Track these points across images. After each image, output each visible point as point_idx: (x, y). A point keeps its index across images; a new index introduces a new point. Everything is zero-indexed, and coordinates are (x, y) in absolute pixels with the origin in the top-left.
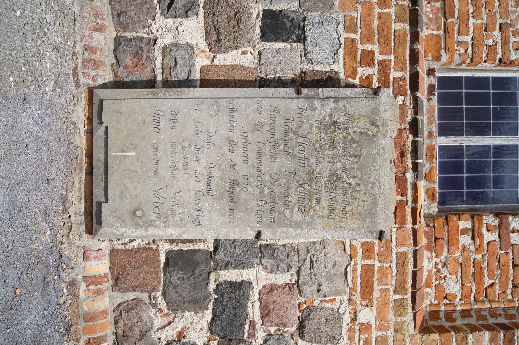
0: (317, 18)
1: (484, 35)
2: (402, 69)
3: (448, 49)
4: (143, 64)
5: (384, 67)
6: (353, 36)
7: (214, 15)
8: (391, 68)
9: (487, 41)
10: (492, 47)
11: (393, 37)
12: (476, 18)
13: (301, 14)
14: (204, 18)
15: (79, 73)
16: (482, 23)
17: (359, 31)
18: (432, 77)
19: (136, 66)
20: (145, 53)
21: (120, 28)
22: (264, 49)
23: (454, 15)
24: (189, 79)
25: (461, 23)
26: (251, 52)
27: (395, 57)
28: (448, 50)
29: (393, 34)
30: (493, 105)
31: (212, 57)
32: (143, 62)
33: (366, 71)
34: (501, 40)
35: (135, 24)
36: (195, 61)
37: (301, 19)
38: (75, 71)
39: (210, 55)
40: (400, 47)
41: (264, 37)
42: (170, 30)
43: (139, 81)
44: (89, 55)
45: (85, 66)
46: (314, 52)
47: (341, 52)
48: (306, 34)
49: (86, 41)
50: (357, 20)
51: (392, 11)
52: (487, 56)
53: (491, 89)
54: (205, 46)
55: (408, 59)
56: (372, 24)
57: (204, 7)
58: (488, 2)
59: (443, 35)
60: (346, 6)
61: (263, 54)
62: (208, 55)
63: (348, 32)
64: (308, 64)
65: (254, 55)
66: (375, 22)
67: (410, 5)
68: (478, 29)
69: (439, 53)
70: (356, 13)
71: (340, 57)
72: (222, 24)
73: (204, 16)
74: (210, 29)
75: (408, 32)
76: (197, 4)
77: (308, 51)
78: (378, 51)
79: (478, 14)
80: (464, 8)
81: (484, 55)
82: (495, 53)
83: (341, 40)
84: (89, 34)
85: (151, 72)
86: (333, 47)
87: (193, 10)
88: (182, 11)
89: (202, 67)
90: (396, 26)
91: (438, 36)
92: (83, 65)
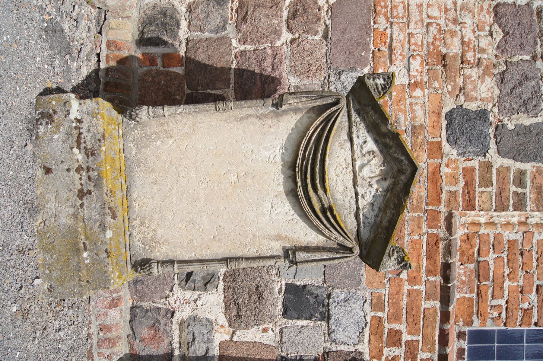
0: (343, 295)
1: (520, 298)
2: (431, 350)
3: (481, 313)
4: (160, 337)
5: (412, 348)
6: (380, 314)
7: (234, 289)
8: (418, 349)
9: (522, 304)
10: (528, 311)
11: (422, 316)
12: (511, 281)
13: (326, 290)
14: (224, 291)
15: (93, 354)
16: (518, 285)
17: (387, 309)
18: (462, 341)
19: (153, 338)
20: (162, 326)
21: (137, 296)
22: (286, 327)
23: (489, 278)
24: (207, 355)
25: (495, 287)
26: (272, 329)
27: (423, 337)
28: (481, 315)
29: (422, 313)
30: (526, 346)
31: (231, 332)
32: (160, 335)
33: (392, 351)
34: (538, 303)
35: (152, 293)
36: (214, 336)
37: (325, 296)
38: (90, 352)
39: (229, 330)
40: (430, 327)
41: (286, 313)
42: (188, 302)
43: (156, 356)
44: (104, 334)
45: (100, 346)
46: (338, 332)
47: (367, 331)
48: (331, 312)
49: (101, 320)
50: (385, 298)
51: (422, 288)
52: (522, 320)
53: (525, 342)
54: (224, 321)
55: (437, 338)
56: (401, 302)
57: (224, 280)
58: (526, 263)
59: (476, 299)
60: (374, 283)
61: (284, 332)
62: (227, 331)
63: (375, 311)
64: (331, 343)
65: (275, 332)
66: (404, 300)
67: (442, 282)
68: (514, 292)
69: (471, 318)
70: (384, 290)
71: (366, 337)
72: (243, 299)
73: (224, 289)
74: (230, 304)
75: (438, 311)
76: (217, 276)
77: (332, 330)
78: (405, 330)
79: (514, 277)
80: (500, 270)
81: (519, 319)
82: (531, 317)
83: (367, 319)
84: (105, 312)
85: (168, 345)
86: (358, 325)
87: (213, 283)
88: (200, 284)
89: (221, 342)
90: (426, 304)
91: (470, 299)
92: (98, 345)
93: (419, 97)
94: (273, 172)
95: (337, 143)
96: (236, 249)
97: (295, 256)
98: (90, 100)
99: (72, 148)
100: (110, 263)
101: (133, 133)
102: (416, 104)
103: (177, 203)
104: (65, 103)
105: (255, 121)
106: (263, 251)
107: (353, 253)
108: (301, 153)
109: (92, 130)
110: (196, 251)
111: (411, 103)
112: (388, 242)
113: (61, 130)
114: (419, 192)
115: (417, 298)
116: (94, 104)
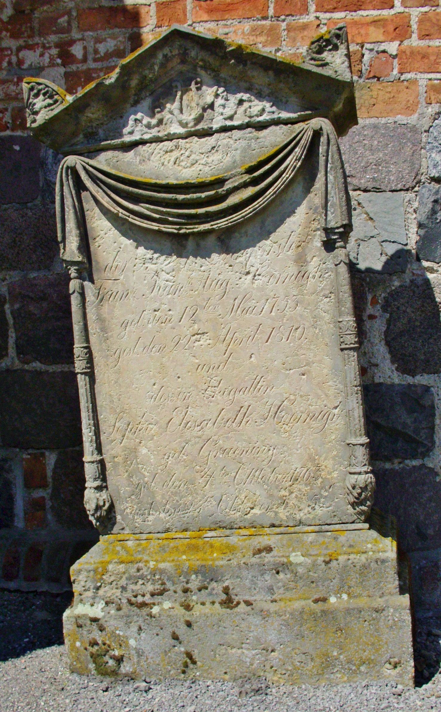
93: (85, 48)
94: (190, 273)
95: (141, 167)
96: (322, 335)
97: (331, 228)
98: (74, 586)
99: (151, 616)
100: (346, 557)
101: (131, 517)
102: (96, 51)
103: (244, 440)
104: (80, 626)
105: (107, 306)
106: (325, 285)
107: (321, 129)
108: (155, 226)
109: (123, 582)
110: (329, 405)
111: (95, 60)
112: (301, 70)
113: (121, 633)
114: (243, 33)
115: (434, 20)
116: (81, 577)
